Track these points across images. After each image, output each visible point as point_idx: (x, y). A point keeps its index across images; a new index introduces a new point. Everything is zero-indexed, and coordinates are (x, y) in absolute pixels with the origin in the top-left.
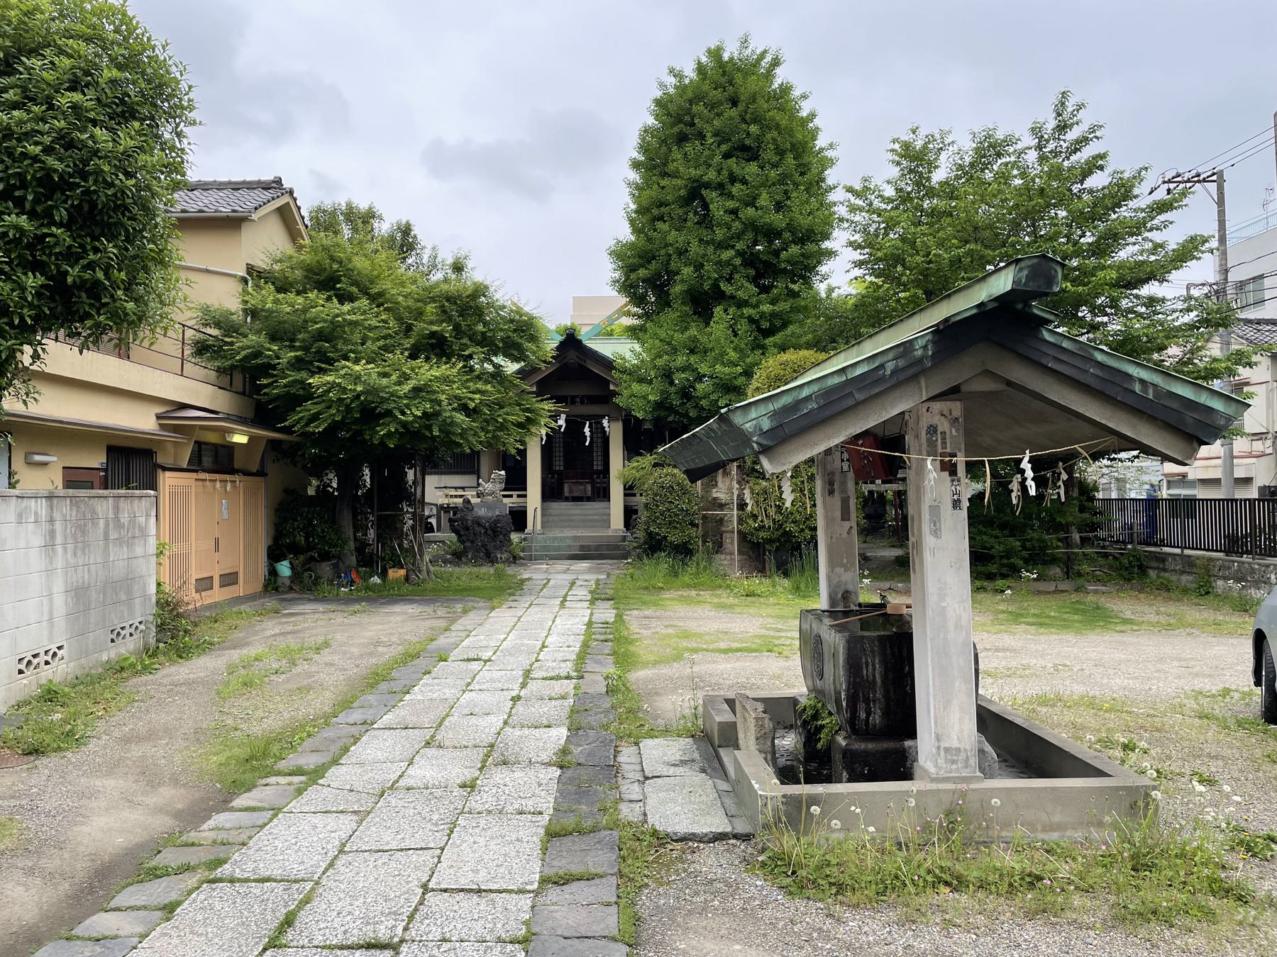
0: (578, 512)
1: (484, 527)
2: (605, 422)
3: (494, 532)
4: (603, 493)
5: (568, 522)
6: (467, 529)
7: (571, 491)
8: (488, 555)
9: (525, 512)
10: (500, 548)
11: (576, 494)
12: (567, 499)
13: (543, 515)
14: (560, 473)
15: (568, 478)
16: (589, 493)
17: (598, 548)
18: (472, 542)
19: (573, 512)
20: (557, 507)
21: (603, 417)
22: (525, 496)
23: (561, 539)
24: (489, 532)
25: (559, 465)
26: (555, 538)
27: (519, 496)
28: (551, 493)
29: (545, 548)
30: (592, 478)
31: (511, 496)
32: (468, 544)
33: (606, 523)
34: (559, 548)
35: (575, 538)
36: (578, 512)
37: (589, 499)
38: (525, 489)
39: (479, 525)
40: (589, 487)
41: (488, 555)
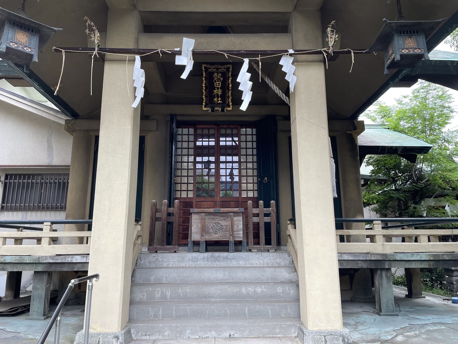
0: (220, 275)
2: (286, 64)
7: (204, 230)
16: (240, 235)
19: (207, 275)
20: (179, 264)
40: (239, 222)
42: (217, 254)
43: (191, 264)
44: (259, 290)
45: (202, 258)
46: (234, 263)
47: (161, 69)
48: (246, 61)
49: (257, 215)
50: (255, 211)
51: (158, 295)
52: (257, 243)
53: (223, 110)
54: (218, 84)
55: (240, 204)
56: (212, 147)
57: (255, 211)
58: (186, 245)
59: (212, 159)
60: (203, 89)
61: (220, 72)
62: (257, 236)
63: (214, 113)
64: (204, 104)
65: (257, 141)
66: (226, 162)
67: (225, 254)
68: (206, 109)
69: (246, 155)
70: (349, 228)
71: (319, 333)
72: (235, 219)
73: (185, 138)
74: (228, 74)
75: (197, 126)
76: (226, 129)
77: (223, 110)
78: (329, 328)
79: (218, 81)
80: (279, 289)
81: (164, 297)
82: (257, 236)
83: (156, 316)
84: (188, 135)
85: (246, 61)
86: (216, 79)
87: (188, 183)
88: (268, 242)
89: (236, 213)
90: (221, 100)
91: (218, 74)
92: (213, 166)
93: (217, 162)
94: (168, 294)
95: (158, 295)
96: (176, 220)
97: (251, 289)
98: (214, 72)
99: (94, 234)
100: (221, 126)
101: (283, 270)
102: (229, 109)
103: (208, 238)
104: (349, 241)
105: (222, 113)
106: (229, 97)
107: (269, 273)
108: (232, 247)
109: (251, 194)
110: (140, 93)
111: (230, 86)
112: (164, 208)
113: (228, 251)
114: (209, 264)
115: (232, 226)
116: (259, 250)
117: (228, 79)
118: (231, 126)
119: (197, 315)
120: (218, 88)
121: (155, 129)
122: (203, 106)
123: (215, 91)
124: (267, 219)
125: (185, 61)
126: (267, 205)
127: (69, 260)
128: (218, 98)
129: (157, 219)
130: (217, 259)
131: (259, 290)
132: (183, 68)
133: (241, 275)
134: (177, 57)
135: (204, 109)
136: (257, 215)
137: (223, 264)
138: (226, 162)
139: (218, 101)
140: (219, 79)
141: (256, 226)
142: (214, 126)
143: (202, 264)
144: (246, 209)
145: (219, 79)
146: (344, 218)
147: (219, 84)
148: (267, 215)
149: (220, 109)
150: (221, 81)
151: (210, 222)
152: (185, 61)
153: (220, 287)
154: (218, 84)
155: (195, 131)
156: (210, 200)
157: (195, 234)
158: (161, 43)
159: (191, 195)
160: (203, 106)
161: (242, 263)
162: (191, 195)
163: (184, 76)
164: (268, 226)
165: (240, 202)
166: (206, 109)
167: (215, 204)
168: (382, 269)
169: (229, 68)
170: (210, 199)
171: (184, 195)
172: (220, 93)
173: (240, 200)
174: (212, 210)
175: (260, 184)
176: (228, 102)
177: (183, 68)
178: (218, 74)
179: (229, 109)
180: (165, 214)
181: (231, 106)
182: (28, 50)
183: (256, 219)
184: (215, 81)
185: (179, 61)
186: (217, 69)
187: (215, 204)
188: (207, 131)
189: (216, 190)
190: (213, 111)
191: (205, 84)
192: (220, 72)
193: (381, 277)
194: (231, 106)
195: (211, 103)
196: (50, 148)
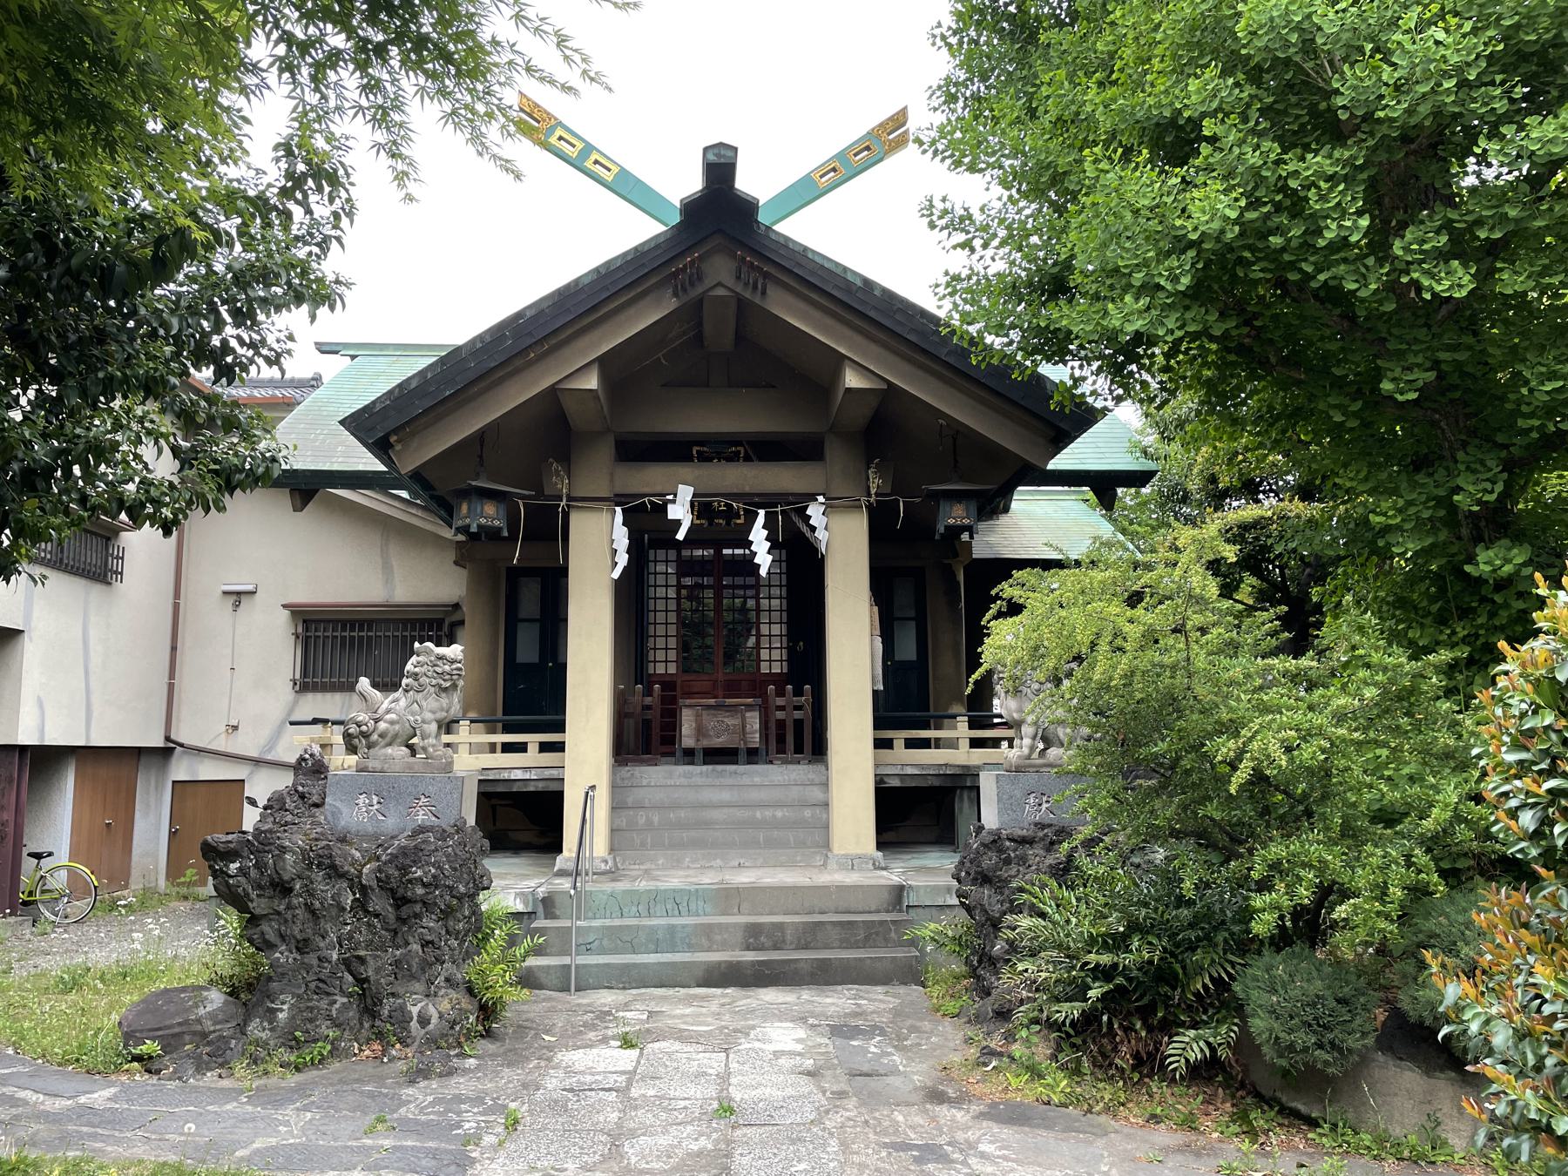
0: (725, 796)
1: (355, 884)
2: (815, 512)
3: (400, 901)
4: (807, 739)
5: (695, 835)
6: (282, 888)
7: (700, 732)
8: (368, 1002)
9: (559, 796)
10: (422, 972)
11: (719, 741)
12: (689, 756)
13: (616, 807)
14: (668, 684)
15: (689, 694)
16: (755, 739)
17: (810, 935)
18: (303, 946)
19: (708, 795)
20: (662, 780)
21: (812, 497)
22: (559, 747)
23: (677, 900)
24: (379, 903)
25: (665, 662)
26: (655, 897)
27: (544, 747)
28: (642, 736)
29: (621, 939)
30: (763, 694)
31: (521, 748)
32: (283, 955)
33: (815, 833)
34: (670, 939)
35: (728, 897)
36: (725, 796)
37: (753, 756)
38: (560, 727)
39: (334, 872)
40: (754, 721)
41: (368, 1002)
42: (720, 767)
43: (683, 781)
44: (779, 814)
45: (699, 771)
46: (746, 780)
47: (647, 525)
48: (762, 513)
49: (782, 708)
50: (780, 701)
51: (642, 821)
52: (781, 750)
53: (728, 524)
57: (780, 701)
58: (672, 754)
62: (781, 740)
65: (788, 574)
66: (734, 587)
67: (733, 767)
70: (938, 728)
71: (846, 856)
72: (748, 714)
78: (859, 851)
80: (807, 813)
81: (649, 823)
82: (781, 740)
83: (643, 844)
85: (762, 513)
88: (799, 749)
89: (749, 707)
92: (709, 593)
94: (656, 819)
95: (642, 821)
96: (655, 715)
97: (768, 813)
99: (570, 737)
101: (815, 788)
103: (706, 743)
104: (937, 747)
107: (795, 792)
108: (742, 756)
109: (776, 669)
110: (623, 559)
112: (637, 698)
113: (708, 386)
114: (709, 781)
115: (744, 727)
116: (786, 762)
119: (696, 844)
124: (798, 714)
125: (680, 511)
126: (798, 692)
127: (505, 775)
129: (627, 715)
130: (721, 775)
131: (779, 814)
132: (678, 523)
133: (755, 795)
134: (670, 506)
136: (782, 708)
137: (730, 781)
138: (734, 587)
141: (781, 724)
143: (700, 781)
144: (766, 701)
146: (932, 712)
148: (797, 708)
151: (711, 721)
152: (680, 511)
153: (726, 810)
157: (687, 737)
158: (646, 479)
159: (672, 669)
161: (757, 780)
162: (672, 669)
163: (680, 536)
164: (799, 724)
168: (963, 788)
171: (660, 669)
174: (712, 701)
175: (791, 651)
177: (678, 523)
180: (639, 708)
182: (496, 523)
183: (780, 715)
185: (674, 512)
190: (710, 524)
193: (961, 800)
196: (387, 568)
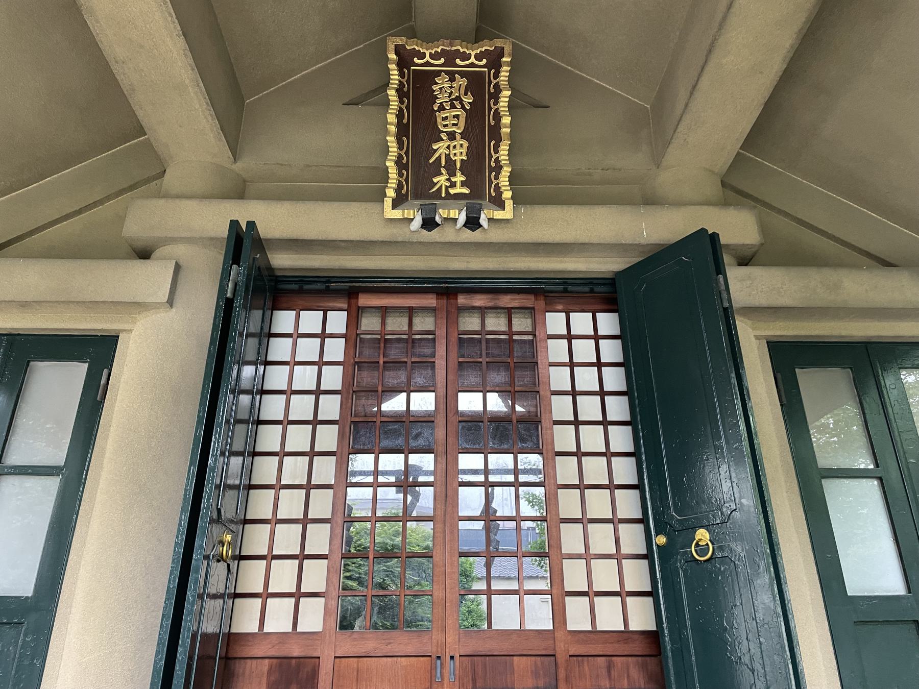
53: (473, 223)
54: (452, 119)
55: (562, 674)
56: (426, 420)
59: (425, 461)
60: (387, 132)
61: (463, 74)
63: (434, 235)
64: (391, 193)
68: (397, 214)
69: (577, 423)
73: (308, 349)
74: (496, 76)
75: (364, 300)
76: (483, 311)
77: (473, 223)
79: (453, 107)
84: (323, 336)
86: (443, 99)
87: (302, 557)
90: (463, 184)
91: (452, 80)
93: (448, 483)
98: (438, 73)
100: (462, 300)
102: (498, 214)
105: (468, 236)
106: (499, 168)
111: (506, 120)
117: (496, 96)
118: (507, 301)
120: (452, 136)
121: (163, 295)
122: (388, 202)
123: (440, 148)
128: (452, 173)
135: (391, 213)
139: (453, 185)
140: (458, 98)
142: (430, 301)
145: (458, 98)
147: (457, 117)
149: (462, 218)
150: (463, 107)
154: (452, 119)
155: (353, 321)
156: (410, 650)
160: (388, 202)
162: (313, 617)
165: (561, 659)
166: (397, 214)
167: (433, 669)
169: (500, 53)
170: (402, 642)
172: (460, 151)
173: (562, 648)
176: (497, 188)
178: (452, 80)
179: (498, 214)
181: (509, 204)
184: (442, 108)
186: (450, 57)
187: (433, 669)
188: (405, 320)
189: (438, 557)
191: (400, 115)
192: (463, 74)
194: (509, 204)
195: (418, 186)
